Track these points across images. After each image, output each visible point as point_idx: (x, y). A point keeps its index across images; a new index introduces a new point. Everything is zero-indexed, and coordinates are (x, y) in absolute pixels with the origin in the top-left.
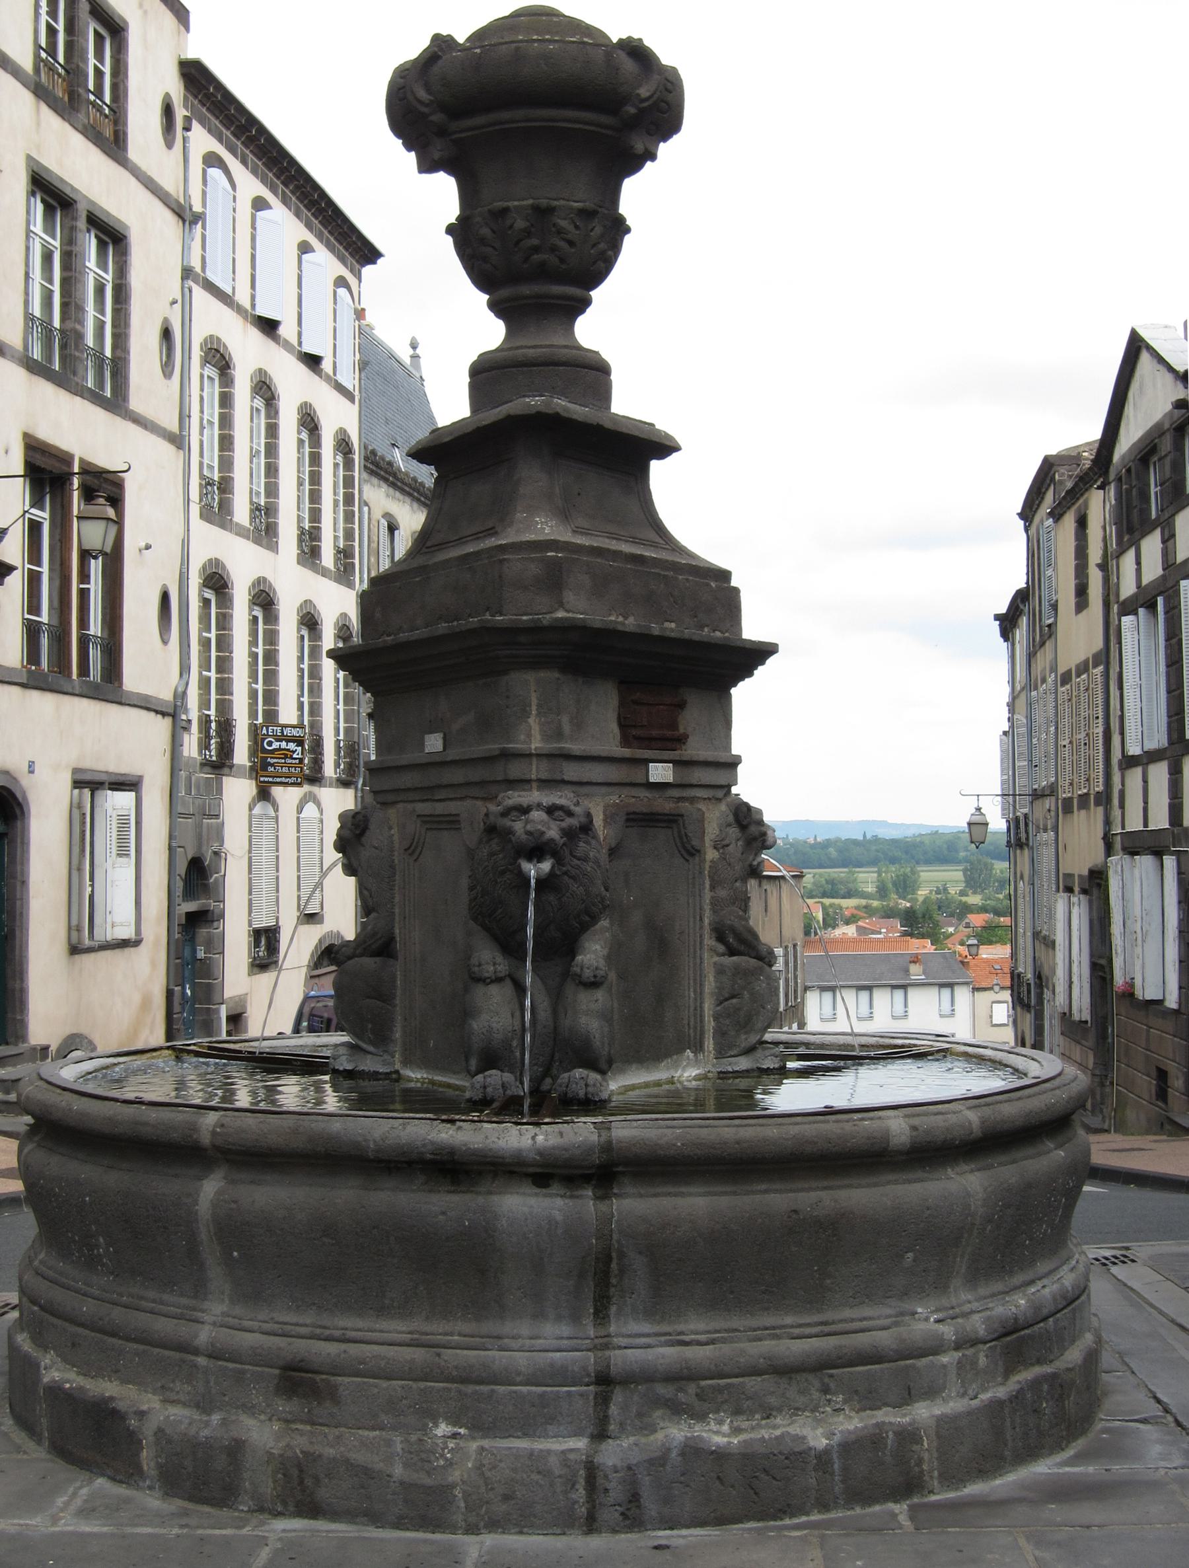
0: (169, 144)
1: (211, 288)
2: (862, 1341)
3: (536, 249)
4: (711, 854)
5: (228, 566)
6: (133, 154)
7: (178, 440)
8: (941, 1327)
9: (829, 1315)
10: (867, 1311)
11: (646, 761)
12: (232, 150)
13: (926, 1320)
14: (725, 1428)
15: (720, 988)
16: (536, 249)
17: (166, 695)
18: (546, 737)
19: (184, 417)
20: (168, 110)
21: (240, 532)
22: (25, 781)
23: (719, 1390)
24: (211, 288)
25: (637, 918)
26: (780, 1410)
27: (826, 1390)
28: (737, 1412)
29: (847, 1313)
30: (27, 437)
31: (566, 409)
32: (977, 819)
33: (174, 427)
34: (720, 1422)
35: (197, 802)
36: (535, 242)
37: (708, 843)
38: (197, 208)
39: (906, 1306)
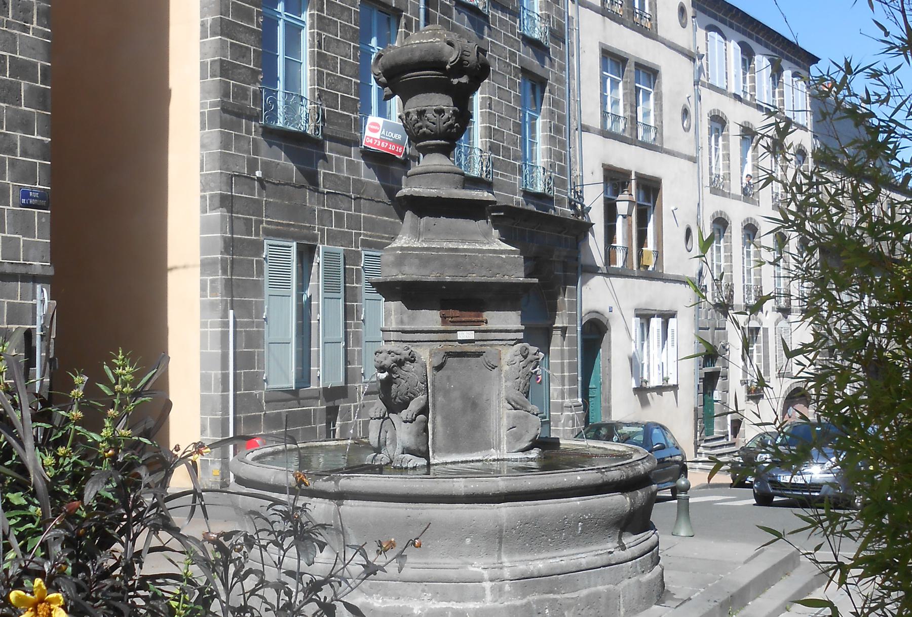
0: (684, 26)
1: (712, 87)
2: (441, 573)
3: (421, 128)
4: (506, 368)
5: (727, 213)
6: (661, 33)
7: (694, 160)
8: (483, 571)
9: (429, 560)
10: (448, 561)
11: (456, 332)
12: (723, 21)
13: (477, 567)
14: (380, 601)
15: (508, 424)
16: (421, 128)
17: (693, 274)
18: (397, 323)
19: (698, 149)
20: (682, 10)
21: (736, 198)
22: (607, 314)
23: (378, 585)
24: (712, 87)
25: (456, 394)
26: (403, 596)
27: (423, 591)
28: (386, 595)
29: (438, 560)
30: (603, 165)
31: (416, 192)
32: (710, 352)
33: (692, 152)
34: (378, 599)
35: (711, 322)
36: (420, 124)
37: (503, 362)
38: (702, 51)
39: (470, 560)
